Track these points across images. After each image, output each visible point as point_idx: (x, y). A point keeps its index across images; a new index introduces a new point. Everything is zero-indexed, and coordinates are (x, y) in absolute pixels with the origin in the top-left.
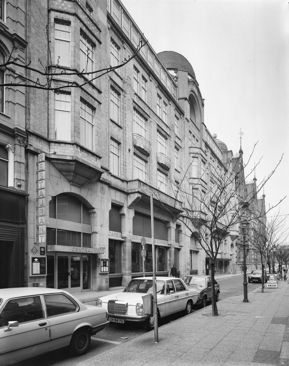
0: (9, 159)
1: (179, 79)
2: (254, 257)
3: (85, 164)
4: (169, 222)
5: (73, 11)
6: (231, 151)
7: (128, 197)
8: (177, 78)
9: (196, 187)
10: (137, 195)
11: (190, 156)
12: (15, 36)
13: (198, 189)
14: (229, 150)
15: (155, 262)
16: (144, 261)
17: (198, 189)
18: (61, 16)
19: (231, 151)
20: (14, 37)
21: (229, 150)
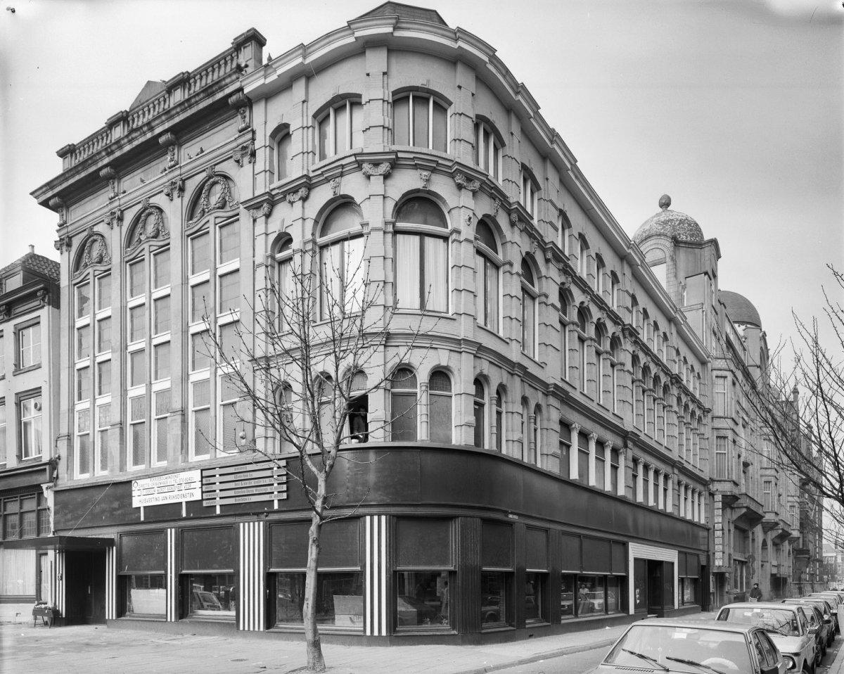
0: (572, 441)
1: (749, 340)
2: (809, 571)
3: (531, 374)
4: (747, 531)
5: (726, 367)
6: (714, 242)
7: (732, 513)
8: (746, 338)
9: (722, 433)
10: (744, 510)
11: (761, 439)
12: (516, 206)
13: (727, 437)
14: (707, 237)
15: (244, 601)
16: (205, 589)
17: (727, 437)
18: (720, 373)
19: (714, 242)
20: (513, 208)
21: (707, 237)
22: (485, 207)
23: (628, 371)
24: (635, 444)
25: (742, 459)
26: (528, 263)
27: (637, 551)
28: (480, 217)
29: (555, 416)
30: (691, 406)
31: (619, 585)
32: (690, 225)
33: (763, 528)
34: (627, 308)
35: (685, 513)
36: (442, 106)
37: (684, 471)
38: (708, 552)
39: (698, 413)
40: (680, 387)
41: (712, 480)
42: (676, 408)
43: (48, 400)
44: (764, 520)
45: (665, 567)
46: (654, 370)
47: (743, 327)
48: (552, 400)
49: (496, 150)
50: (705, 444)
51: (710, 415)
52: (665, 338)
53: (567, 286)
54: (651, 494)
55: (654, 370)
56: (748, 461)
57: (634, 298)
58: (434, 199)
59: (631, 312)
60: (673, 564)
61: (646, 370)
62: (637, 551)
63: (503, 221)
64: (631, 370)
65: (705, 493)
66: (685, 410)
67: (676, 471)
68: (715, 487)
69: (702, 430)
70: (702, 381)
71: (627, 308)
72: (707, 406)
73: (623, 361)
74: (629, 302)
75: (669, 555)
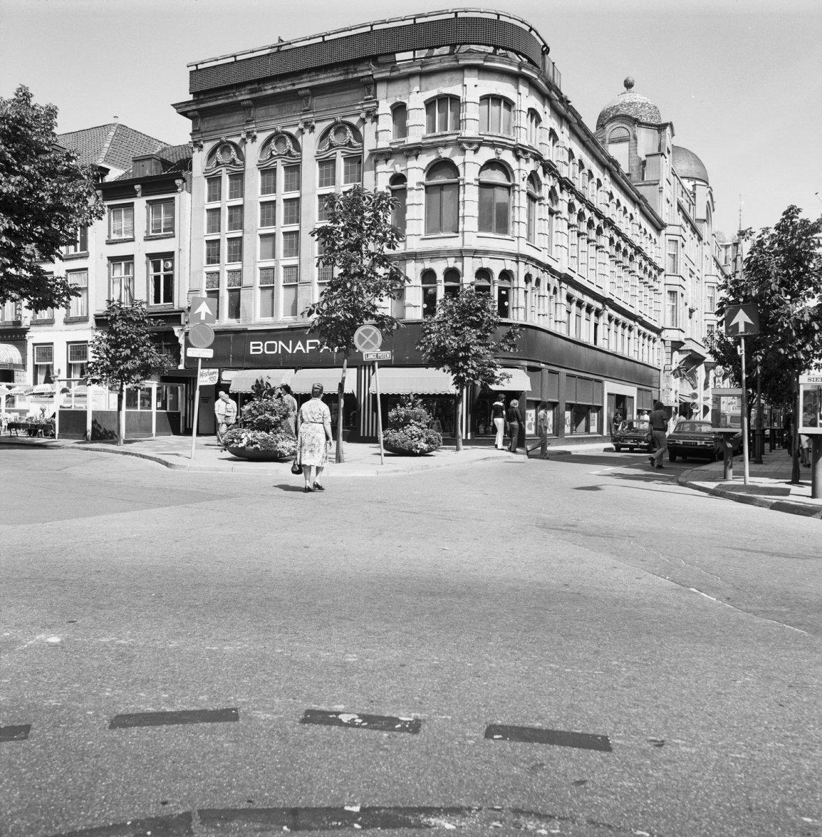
22: (530, 166)
23: (565, 219)
24: (610, 307)
25: (688, 306)
26: (552, 194)
27: (611, 387)
28: (529, 173)
29: (564, 293)
30: (649, 268)
31: (197, 312)
32: (650, 108)
33: (706, 367)
34: (565, 163)
35: (623, 348)
36: (509, 104)
37: (643, 323)
38: (659, 388)
39: (654, 272)
40: (612, 229)
41: (663, 329)
42: (607, 248)
43: (107, 229)
44: (706, 361)
45: (628, 400)
46: (623, 245)
47: (692, 183)
48: (564, 285)
49: (536, 122)
50: (657, 298)
51: (663, 273)
52: (599, 184)
53: (572, 201)
54: (613, 340)
55: (588, 214)
56: (694, 308)
57: (570, 152)
58: (511, 176)
59: (567, 165)
60: (633, 398)
61: (581, 216)
62: (611, 387)
63: (540, 172)
64: (567, 217)
65: (659, 340)
66: (649, 277)
67: (637, 323)
68: (664, 335)
69: (656, 286)
70: (657, 245)
71: (565, 163)
72: (661, 266)
73: (603, 245)
74: (566, 157)
75: (630, 390)
